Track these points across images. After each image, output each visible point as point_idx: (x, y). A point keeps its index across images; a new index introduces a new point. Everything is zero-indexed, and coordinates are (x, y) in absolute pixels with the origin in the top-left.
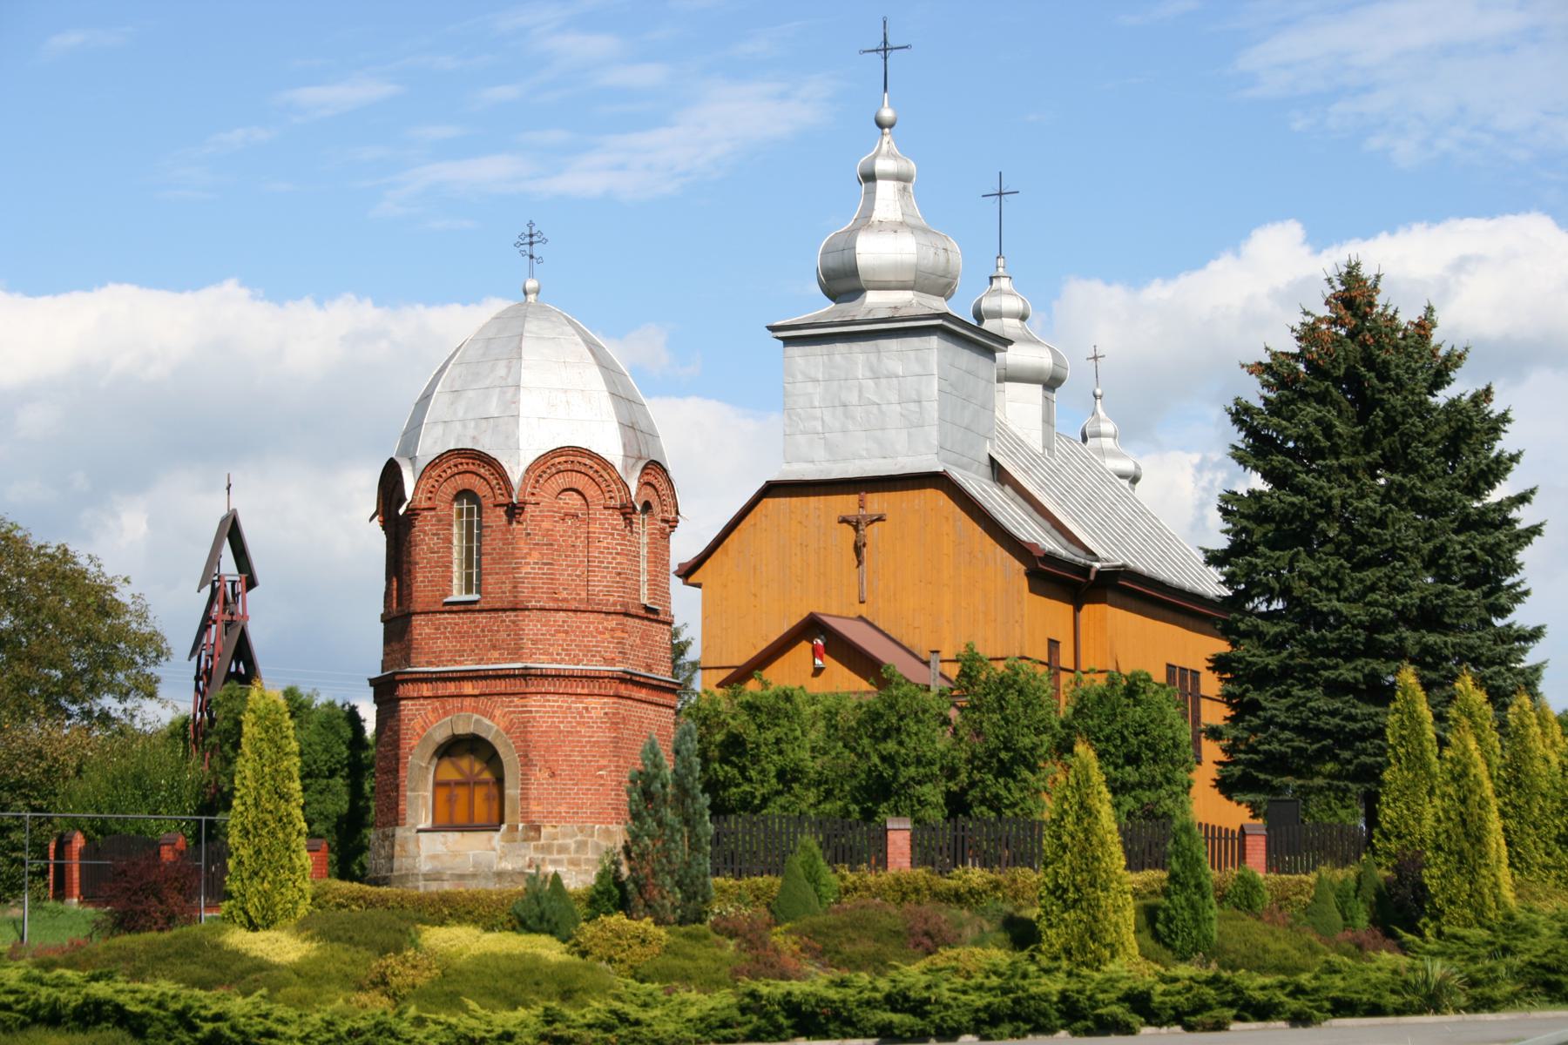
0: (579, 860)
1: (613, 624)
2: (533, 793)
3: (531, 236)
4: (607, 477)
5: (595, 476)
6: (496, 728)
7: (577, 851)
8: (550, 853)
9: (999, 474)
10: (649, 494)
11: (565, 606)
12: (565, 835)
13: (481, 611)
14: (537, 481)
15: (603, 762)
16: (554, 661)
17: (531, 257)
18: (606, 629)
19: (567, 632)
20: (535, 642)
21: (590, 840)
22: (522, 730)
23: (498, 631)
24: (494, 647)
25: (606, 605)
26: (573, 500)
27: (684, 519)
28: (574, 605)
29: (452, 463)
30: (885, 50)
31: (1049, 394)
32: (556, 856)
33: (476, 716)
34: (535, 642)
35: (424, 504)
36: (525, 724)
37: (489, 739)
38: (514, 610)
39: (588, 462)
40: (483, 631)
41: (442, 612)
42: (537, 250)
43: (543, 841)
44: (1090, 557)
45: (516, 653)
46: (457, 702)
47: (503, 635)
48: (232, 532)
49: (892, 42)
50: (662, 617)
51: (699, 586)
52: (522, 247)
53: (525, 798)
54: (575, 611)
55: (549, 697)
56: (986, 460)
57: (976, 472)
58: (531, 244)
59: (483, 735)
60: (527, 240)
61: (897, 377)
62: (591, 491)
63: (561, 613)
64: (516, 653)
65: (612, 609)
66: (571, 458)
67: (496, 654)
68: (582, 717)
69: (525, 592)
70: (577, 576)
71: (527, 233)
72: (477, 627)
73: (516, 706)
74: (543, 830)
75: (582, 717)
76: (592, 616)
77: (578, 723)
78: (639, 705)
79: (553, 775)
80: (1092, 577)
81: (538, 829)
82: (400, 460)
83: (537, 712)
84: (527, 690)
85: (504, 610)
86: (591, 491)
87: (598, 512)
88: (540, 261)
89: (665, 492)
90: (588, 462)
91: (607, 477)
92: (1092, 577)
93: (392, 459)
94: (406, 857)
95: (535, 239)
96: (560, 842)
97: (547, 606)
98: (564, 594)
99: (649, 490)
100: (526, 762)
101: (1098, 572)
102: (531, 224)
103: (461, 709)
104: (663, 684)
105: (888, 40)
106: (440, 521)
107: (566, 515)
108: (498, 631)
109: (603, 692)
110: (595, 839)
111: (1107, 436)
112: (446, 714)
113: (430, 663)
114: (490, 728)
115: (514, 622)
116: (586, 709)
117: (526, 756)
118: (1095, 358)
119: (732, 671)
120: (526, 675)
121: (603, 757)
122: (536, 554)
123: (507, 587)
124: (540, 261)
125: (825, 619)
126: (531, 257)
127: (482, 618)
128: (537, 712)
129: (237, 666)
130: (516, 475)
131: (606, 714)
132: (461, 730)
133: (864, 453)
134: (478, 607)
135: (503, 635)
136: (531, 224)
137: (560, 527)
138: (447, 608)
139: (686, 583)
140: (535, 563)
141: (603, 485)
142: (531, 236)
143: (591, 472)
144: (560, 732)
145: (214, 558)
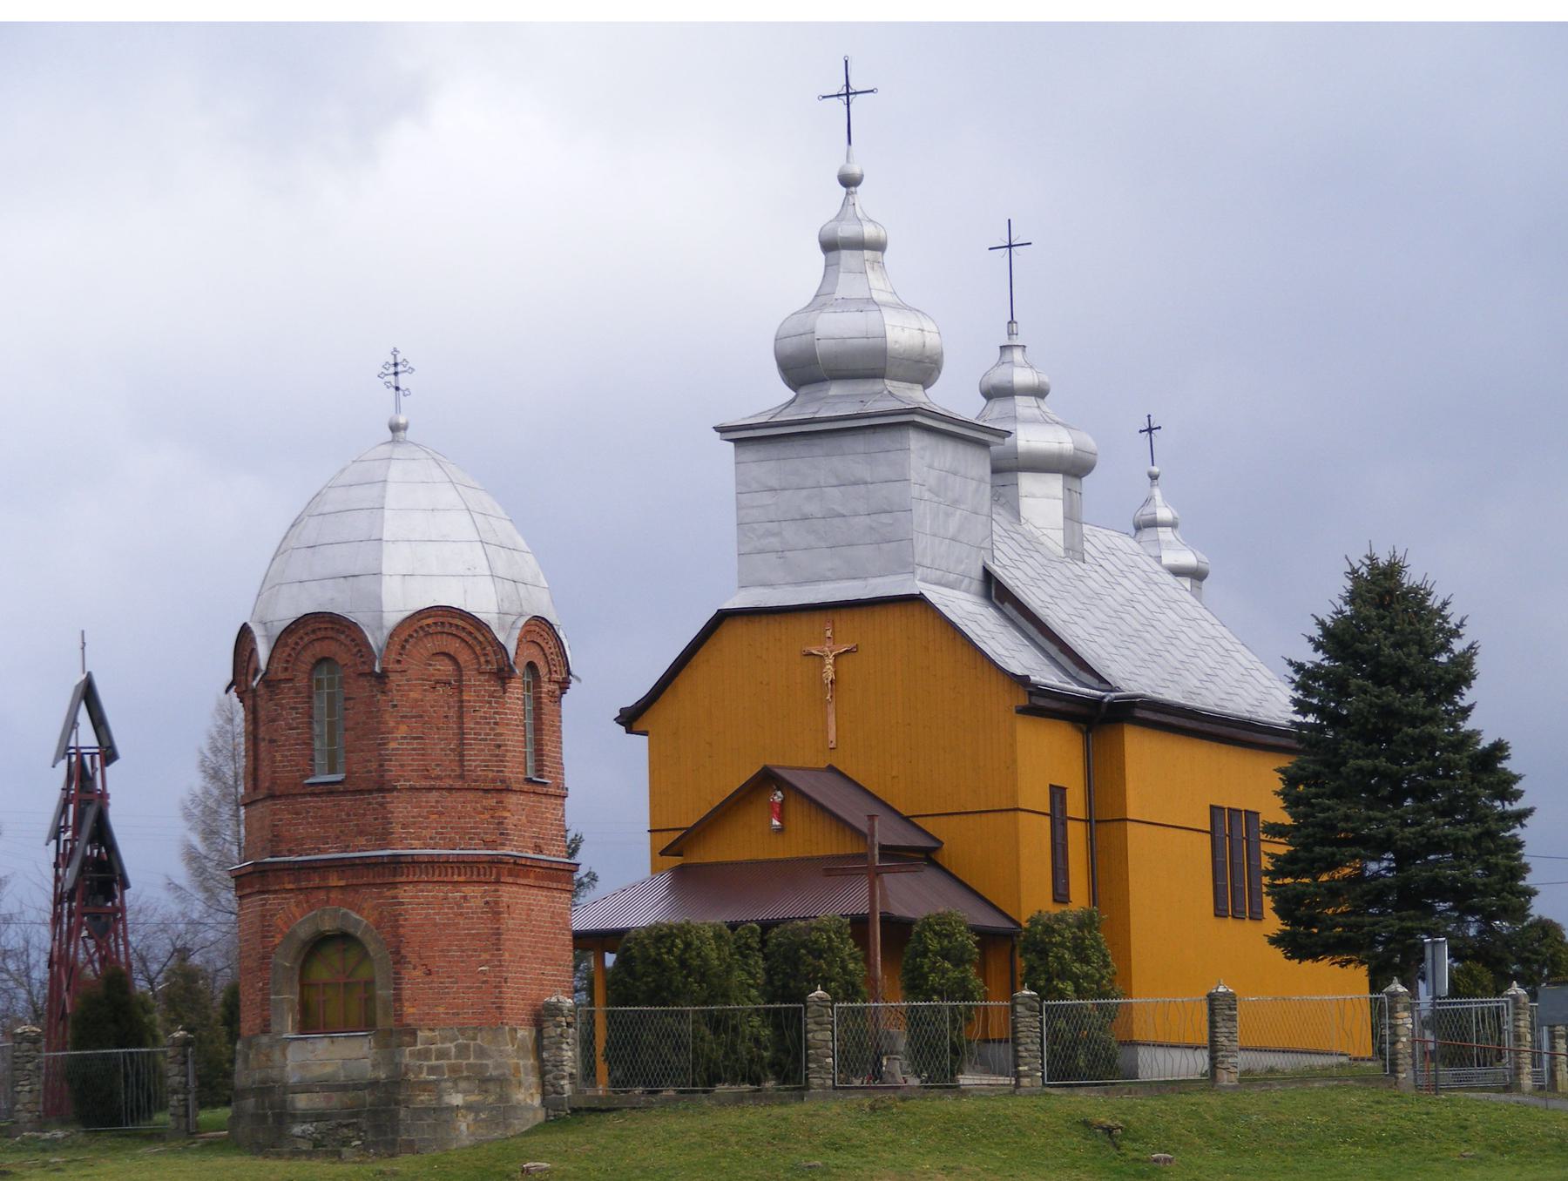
0: (460, 1066)
1: (493, 802)
2: (407, 994)
3: (396, 365)
4: (481, 638)
5: (468, 639)
6: (366, 922)
7: (457, 1057)
8: (427, 1058)
9: (995, 591)
10: (533, 654)
11: (438, 783)
12: (444, 1040)
13: (345, 792)
14: (403, 647)
15: (485, 956)
16: (426, 846)
17: (397, 388)
18: (485, 808)
19: (441, 814)
20: (404, 826)
21: (472, 1043)
22: (391, 922)
23: (364, 815)
24: (361, 833)
25: (484, 781)
26: (444, 668)
27: (579, 680)
28: (448, 783)
29: (310, 628)
30: (848, 94)
31: (1074, 483)
32: (433, 1062)
33: (344, 910)
34: (404, 826)
35: (282, 676)
36: (395, 918)
37: (359, 934)
38: (381, 790)
39: (460, 623)
40: (348, 815)
41: (304, 795)
42: (403, 381)
43: (419, 1047)
44: (1103, 686)
45: (384, 838)
46: (322, 895)
47: (370, 819)
48: (88, 694)
49: (854, 87)
50: (551, 790)
51: (645, 733)
52: (387, 379)
53: (398, 998)
54: (450, 789)
55: (421, 886)
56: (977, 573)
57: (967, 591)
58: (396, 374)
59: (351, 930)
60: (392, 370)
61: (866, 483)
62: (464, 657)
63: (434, 793)
64: (384, 838)
65: (491, 786)
66: (441, 619)
67: (362, 841)
68: (460, 907)
69: (393, 770)
70: (451, 750)
71: (392, 362)
72: (342, 810)
73: (386, 898)
74: (420, 1034)
75: (460, 907)
76: (470, 796)
77: (456, 915)
78: (527, 890)
79: (429, 973)
80: (1103, 710)
81: (413, 1033)
82: (251, 624)
83: (410, 903)
84: (399, 879)
85: (370, 792)
86: (464, 657)
87: (472, 679)
88: (407, 393)
89: (550, 648)
90: (460, 623)
91: (481, 638)
92: (1103, 710)
93: (245, 624)
94: (272, 1068)
95: (400, 368)
96: (439, 1045)
97: (418, 785)
98: (437, 772)
99: (534, 650)
100: (399, 960)
101: (1110, 703)
102: (395, 352)
103: (327, 902)
104: (554, 866)
105: (851, 83)
106: (298, 693)
107: (438, 682)
108: (364, 815)
109: (482, 878)
110: (479, 1042)
111: (1164, 524)
112: (311, 908)
113: (291, 852)
114: (358, 922)
115: (381, 804)
116: (465, 898)
117: (398, 952)
118: (1150, 430)
119: (678, 834)
120: (396, 863)
121: (485, 951)
122: (403, 728)
123: (373, 765)
124: (407, 393)
125: (776, 770)
126: (397, 388)
127: (347, 801)
128: (410, 903)
129: (92, 852)
130: (376, 639)
131: (487, 903)
132: (328, 926)
133: (829, 574)
134: (341, 788)
135: (370, 819)
136: (395, 352)
137: (430, 697)
138: (309, 789)
139: (629, 731)
140: (405, 738)
141: (478, 649)
142: (396, 365)
143: (463, 635)
144: (436, 925)
145: (72, 724)
